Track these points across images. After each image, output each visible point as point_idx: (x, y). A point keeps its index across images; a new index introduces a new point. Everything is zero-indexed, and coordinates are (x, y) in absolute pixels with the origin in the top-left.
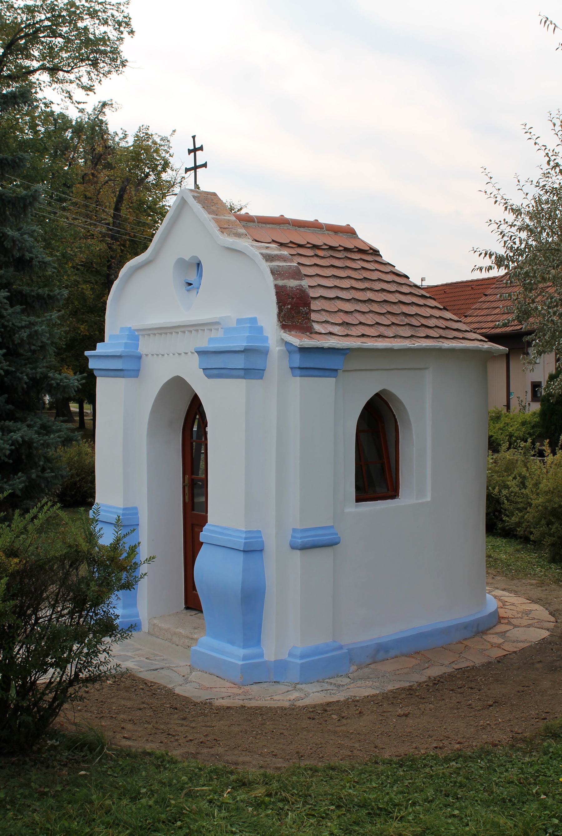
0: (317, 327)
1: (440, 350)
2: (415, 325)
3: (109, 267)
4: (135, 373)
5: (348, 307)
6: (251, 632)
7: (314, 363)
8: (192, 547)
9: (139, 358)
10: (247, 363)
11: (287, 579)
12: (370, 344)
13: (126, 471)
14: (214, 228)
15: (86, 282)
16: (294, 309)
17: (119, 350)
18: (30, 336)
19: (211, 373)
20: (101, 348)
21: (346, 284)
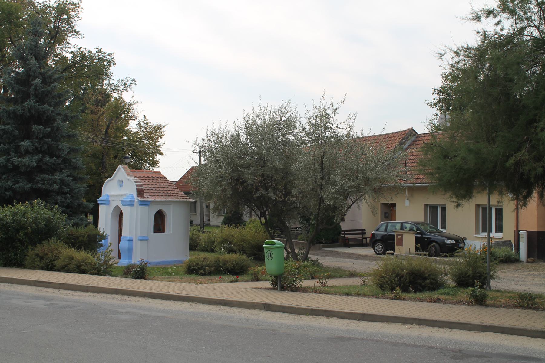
0: (145, 196)
1: (173, 201)
2: (168, 195)
3: (103, 156)
4: (108, 204)
5: (154, 192)
6: (130, 257)
7: (143, 203)
8: (120, 241)
9: (109, 201)
10: (130, 203)
11: (138, 247)
12: (156, 200)
13: (105, 223)
14: (125, 174)
15: (92, 162)
16: (140, 193)
17: (105, 199)
18: (78, 191)
19: (124, 205)
20: (100, 199)
21: (155, 186)
